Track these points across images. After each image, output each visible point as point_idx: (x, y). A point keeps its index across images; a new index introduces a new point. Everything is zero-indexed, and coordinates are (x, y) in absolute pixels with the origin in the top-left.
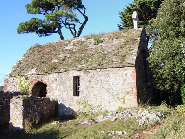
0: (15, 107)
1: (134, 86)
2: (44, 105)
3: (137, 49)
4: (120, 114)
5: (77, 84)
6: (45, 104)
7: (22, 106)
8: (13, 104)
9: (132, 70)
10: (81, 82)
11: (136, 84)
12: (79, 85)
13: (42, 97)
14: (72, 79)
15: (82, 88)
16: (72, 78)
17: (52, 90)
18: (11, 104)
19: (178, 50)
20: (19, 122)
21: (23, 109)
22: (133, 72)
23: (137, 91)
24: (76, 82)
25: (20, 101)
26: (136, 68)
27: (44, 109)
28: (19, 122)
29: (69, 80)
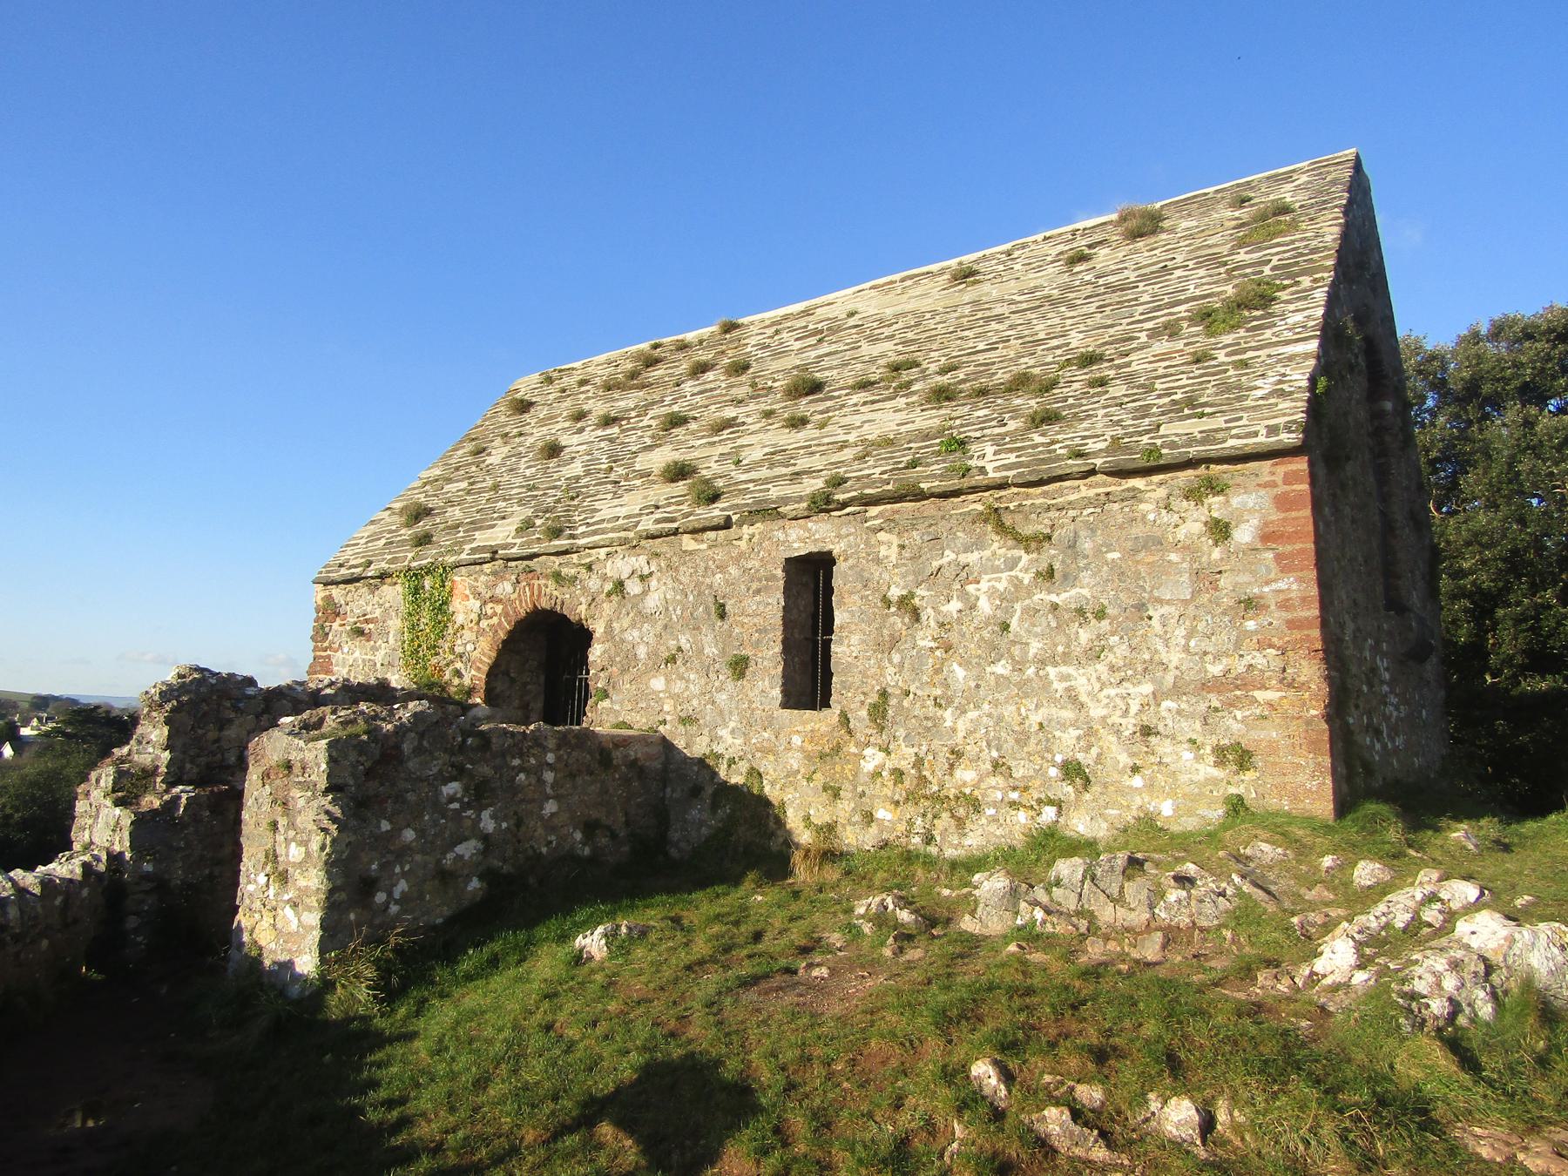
0: (274, 802)
1: (1297, 634)
2: (541, 781)
3: (1320, 312)
4: (1167, 879)
5: (815, 616)
6: (549, 776)
7: (327, 791)
8: (266, 776)
9: (1273, 485)
10: (841, 603)
11: (1314, 612)
12: (829, 628)
13: (527, 724)
14: (773, 577)
15: (847, 648)
16: (779, 573)
17: (624, 671)
18: (253, 776)
19: (529, 1036)
20: (294, 926)
21: (334, 820)
22: (1282, 502)
23: (1329, 679)
24: (805, 600)
25: (315, 756)
26: (1311, 464)
27: (541, 818)
28: (294, 926)
29: (755, 586)
